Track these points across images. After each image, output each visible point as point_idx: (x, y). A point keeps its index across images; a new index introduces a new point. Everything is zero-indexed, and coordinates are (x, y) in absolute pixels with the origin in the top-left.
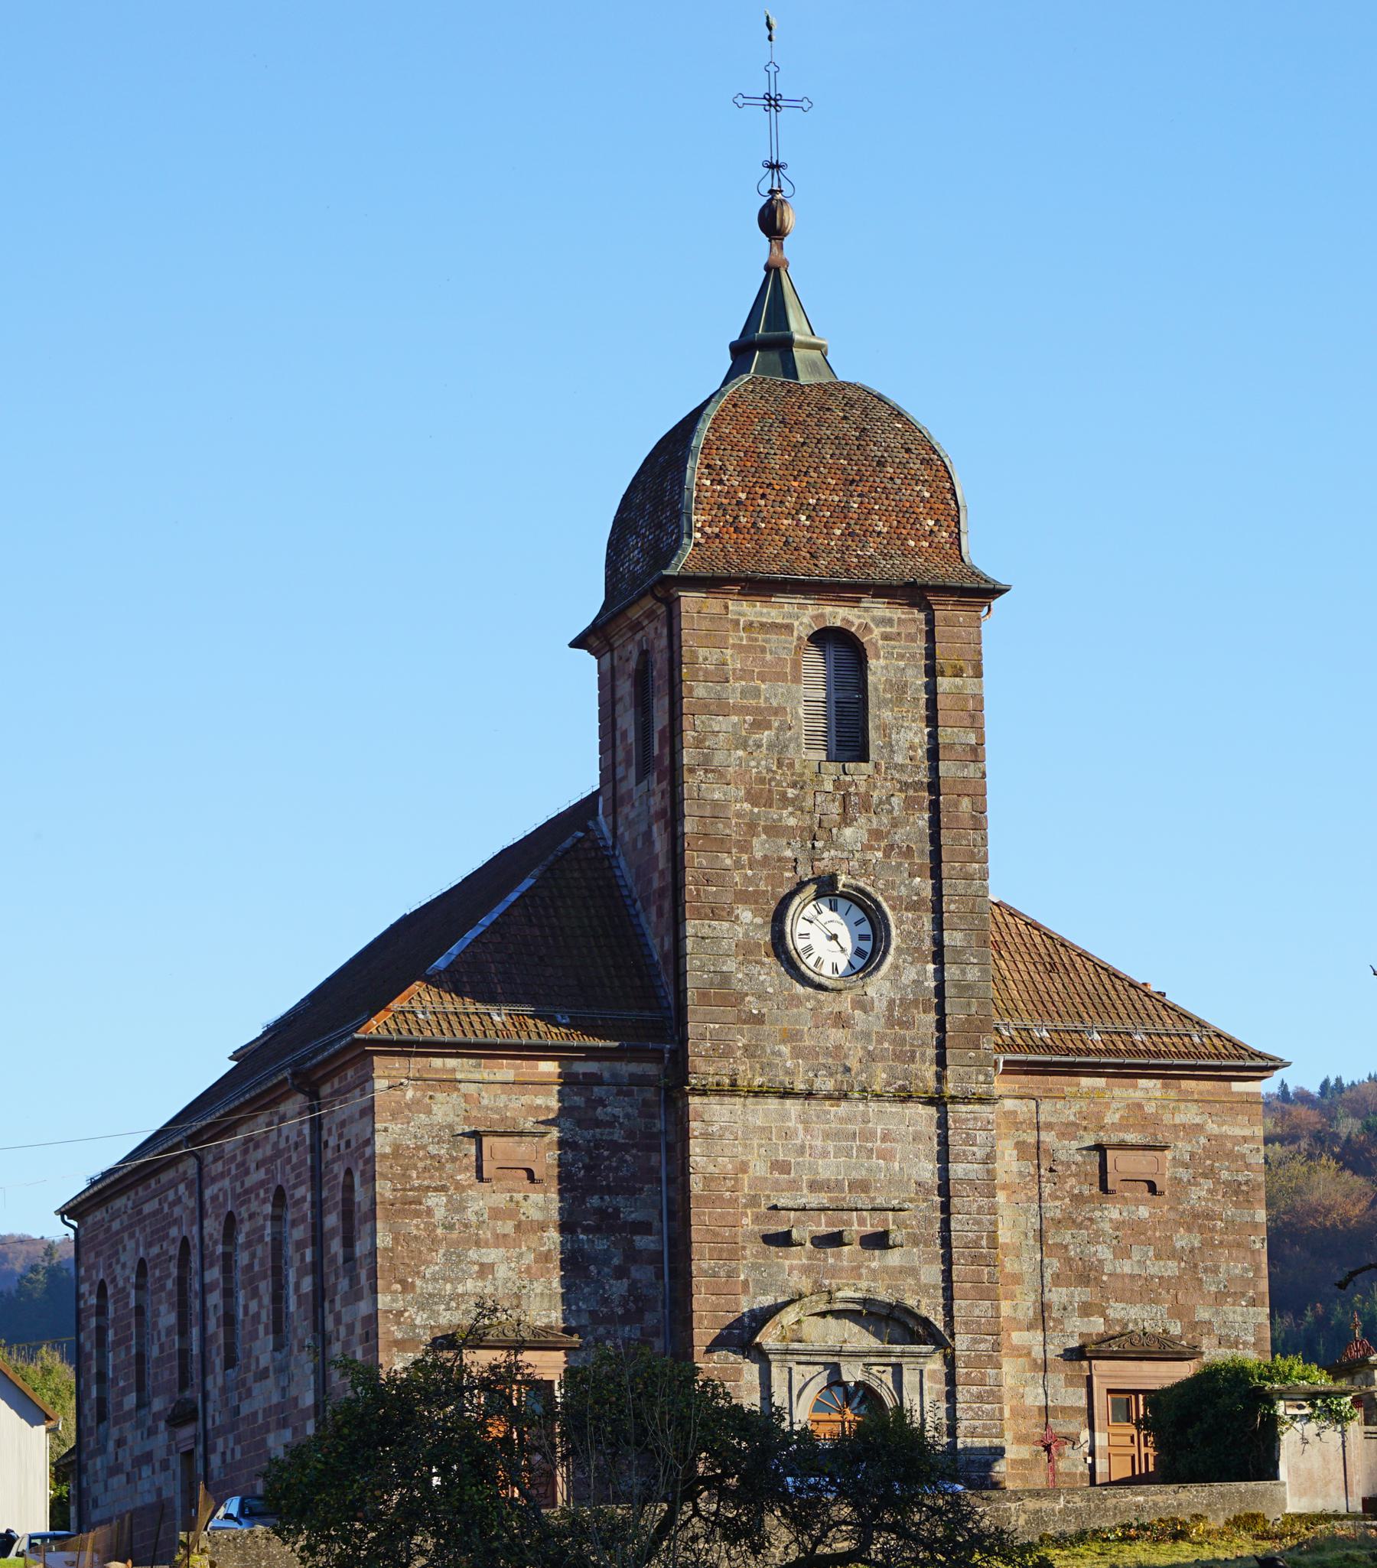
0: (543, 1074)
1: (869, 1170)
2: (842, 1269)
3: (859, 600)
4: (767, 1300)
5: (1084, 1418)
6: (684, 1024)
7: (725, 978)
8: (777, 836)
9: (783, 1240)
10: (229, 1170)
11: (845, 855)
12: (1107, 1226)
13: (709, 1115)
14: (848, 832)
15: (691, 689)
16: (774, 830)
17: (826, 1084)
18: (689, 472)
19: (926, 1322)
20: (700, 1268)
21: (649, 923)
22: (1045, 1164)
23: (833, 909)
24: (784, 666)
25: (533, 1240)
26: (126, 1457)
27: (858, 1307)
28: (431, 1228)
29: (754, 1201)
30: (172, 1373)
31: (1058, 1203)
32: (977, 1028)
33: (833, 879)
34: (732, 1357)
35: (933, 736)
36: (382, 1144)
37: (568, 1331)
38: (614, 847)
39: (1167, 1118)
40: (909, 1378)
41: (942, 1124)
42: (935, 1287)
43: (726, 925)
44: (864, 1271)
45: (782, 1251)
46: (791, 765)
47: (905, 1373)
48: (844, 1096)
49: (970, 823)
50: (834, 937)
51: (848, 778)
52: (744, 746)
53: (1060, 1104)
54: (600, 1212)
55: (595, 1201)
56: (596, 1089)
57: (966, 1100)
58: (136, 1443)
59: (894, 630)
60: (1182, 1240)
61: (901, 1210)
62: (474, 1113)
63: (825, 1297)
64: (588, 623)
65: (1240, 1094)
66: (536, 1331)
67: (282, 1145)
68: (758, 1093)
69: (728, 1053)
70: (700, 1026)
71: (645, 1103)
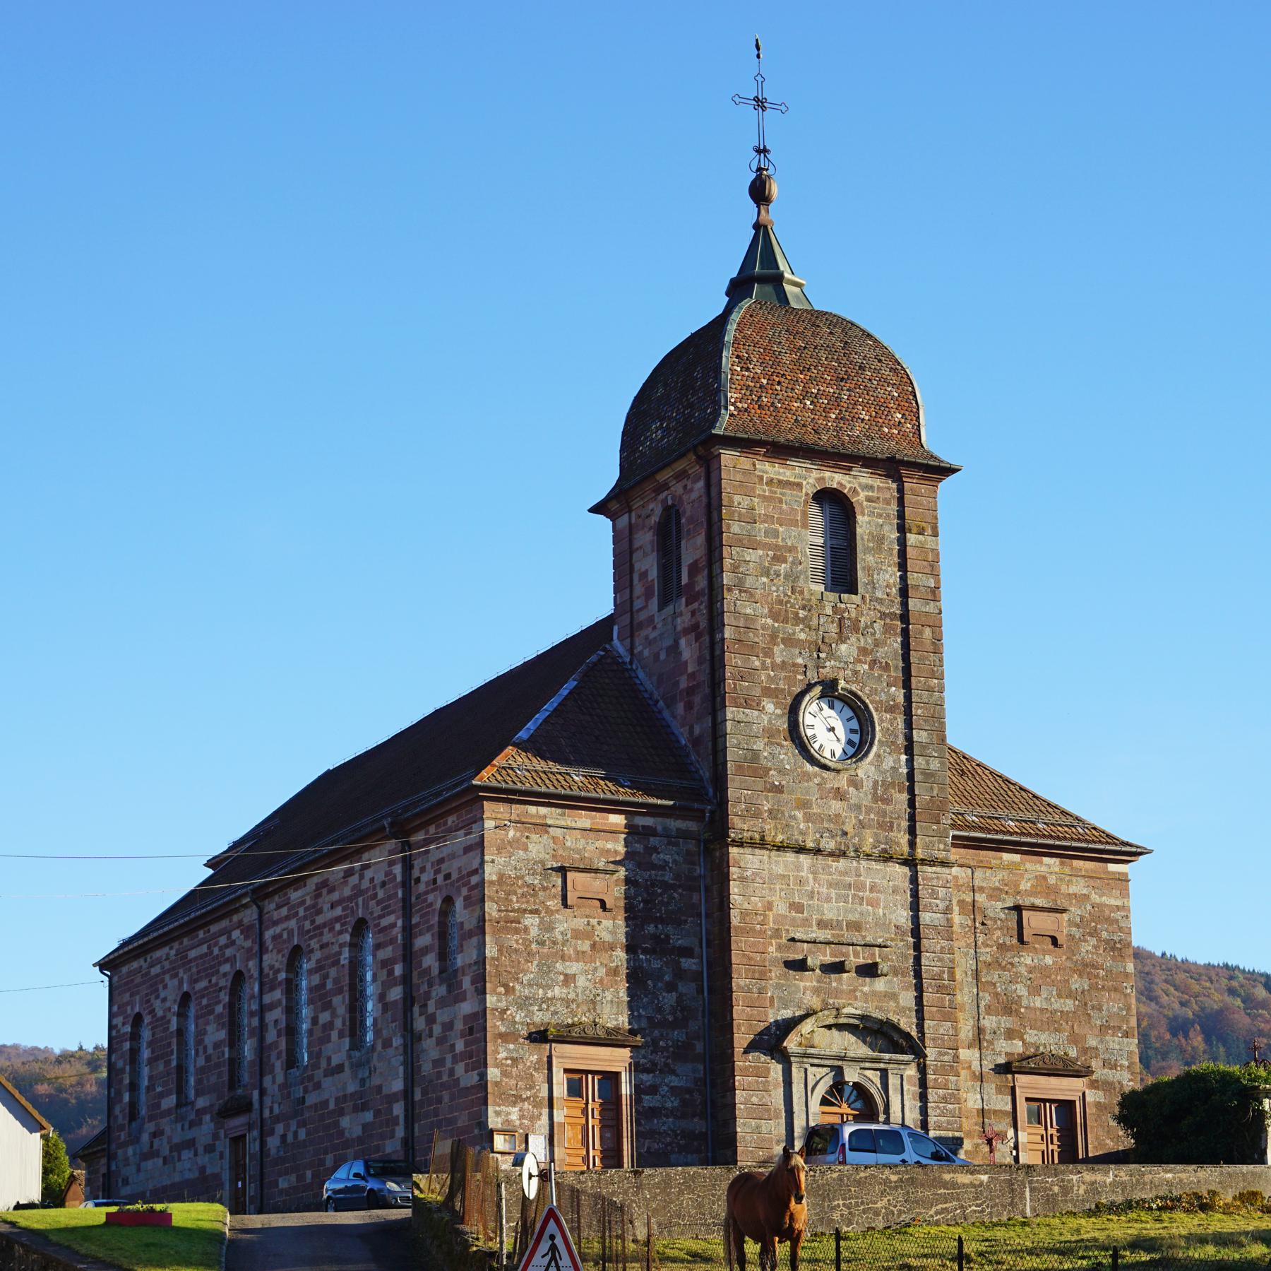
0: (612, 824)
1: (861, 914)
2: (842, 991)
3: (850, 469)
4: (787, 1014)
5: (1009, 1120)
6: (725, 789)
7: (755, 755)
8: (791, 646)
9: (800, 966)
10: (297, 913)
11: (842, 665)
12: (1023, 970)
13: (744, 862)
14: (843, 647)
15: (729, 526)
16: (789, 642)
17: (829, 844)
18: (724, 360)
19: (907, 1036)
20: (738, 985)
21: (675, 717)
22: (979, 919)
23: (831, 707)
24: (796, 515)
25: (605, 957)
26: (163, 1145)
27: (857, 1022)
28: (527, 943)
29: (777, 933)
30: (220, 1075)
31: (988, 950)
32: (937, 809)
33: (834, 682)
34: (763, 1058)
35: (904, 579)
36: (490, 873)
37: (632, 1032)
38: (631, 663)
39: (1064, 889)
40: (893, 1081)
41: (914, 880)
42: (910, 1009)
43: (756, 713)
44: (858, 994)
45: (798, 975)
46: (802, 592)
47: (890, 1076)
48: (843, 854)
49: (931, 648)
50: (832, 729)
51: (843, 606)
52: (767, 574)
53: (989, 872)
54: (655, 937)
55: (651, 928)
56: (652, 839)
57: (932, 862)
58: (174, 1132)
59: (875, 494)
60: (1077, 983)
61: (885, 947)
62: (560, 852)
63: (834, 1013)
64: (603, 496)
65: (1114, 873)
66: (609, 1031)
67: (365, 884)
68: (780, 848)
69: (757, 815)
70: (737, 790)
71: (688, 853)
